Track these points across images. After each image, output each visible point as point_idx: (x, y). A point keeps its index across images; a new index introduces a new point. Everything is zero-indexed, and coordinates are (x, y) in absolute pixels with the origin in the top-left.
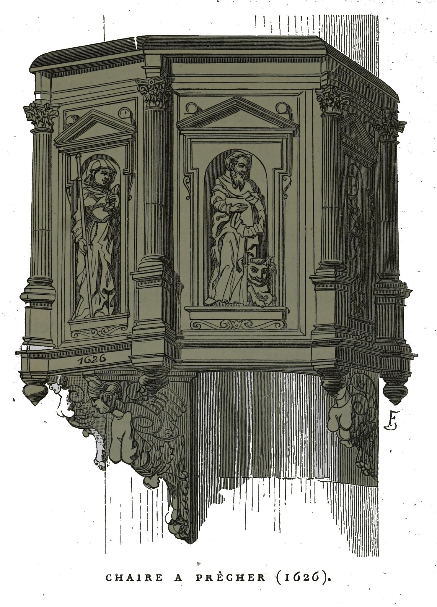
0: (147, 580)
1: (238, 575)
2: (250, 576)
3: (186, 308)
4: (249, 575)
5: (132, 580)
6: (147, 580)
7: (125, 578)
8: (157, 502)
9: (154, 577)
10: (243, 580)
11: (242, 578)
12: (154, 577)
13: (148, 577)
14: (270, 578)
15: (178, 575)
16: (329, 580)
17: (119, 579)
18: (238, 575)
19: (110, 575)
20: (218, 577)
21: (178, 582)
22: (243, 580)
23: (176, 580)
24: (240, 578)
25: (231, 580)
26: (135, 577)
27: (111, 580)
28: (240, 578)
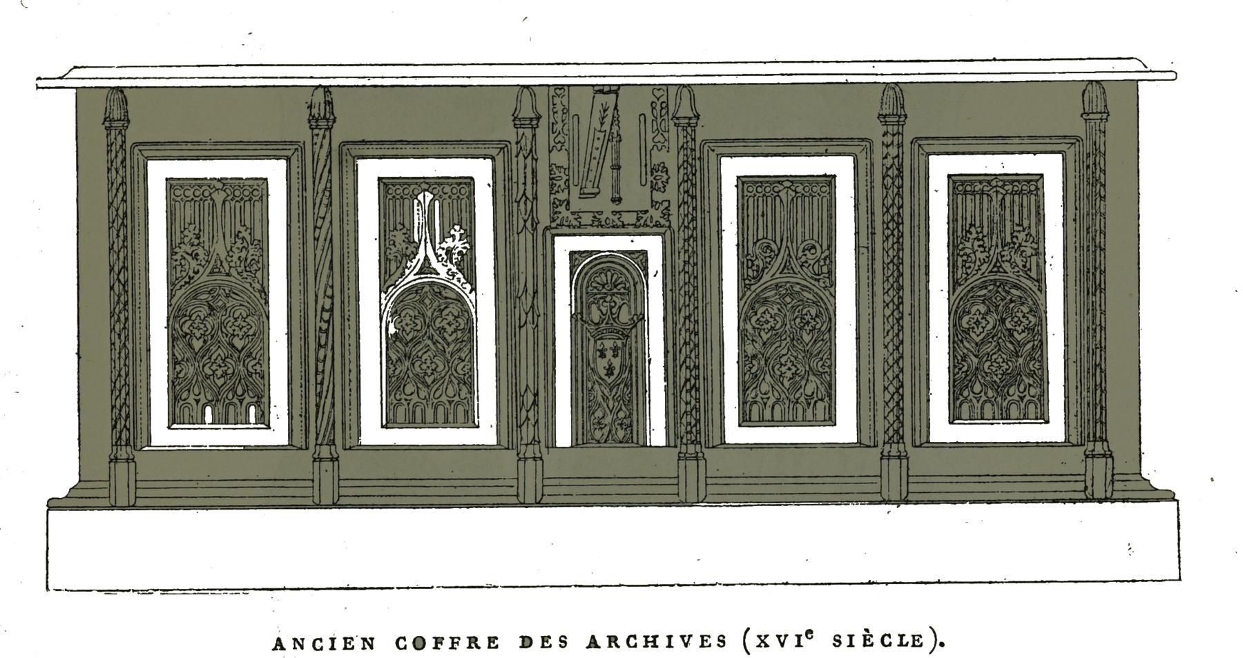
0: (470, 647)
1: (646, 637)
2: (545, 639)
3: (1172, 76)
4: (345, 639)
5: (283, 649)
6: (470, 647)
7: (695, 641)
8: (66, 478)
9: (483, 642)
10: (655, 646)
11: (654, 641)
12: (483, 642)
13: (613, 640)
14: (734, 641)
15: (593, 637)
16: (942, 644)
17: (650, 639)
18: (646, 637)
19: (321, 640)
20: (865, 640)
21: (279, 652)
22: (655, 646)
23: (275, 649)
24: (651, 642)
25: (635, 646)
26: (677, 641)
27: (890, 644)
28: (651, 642)
